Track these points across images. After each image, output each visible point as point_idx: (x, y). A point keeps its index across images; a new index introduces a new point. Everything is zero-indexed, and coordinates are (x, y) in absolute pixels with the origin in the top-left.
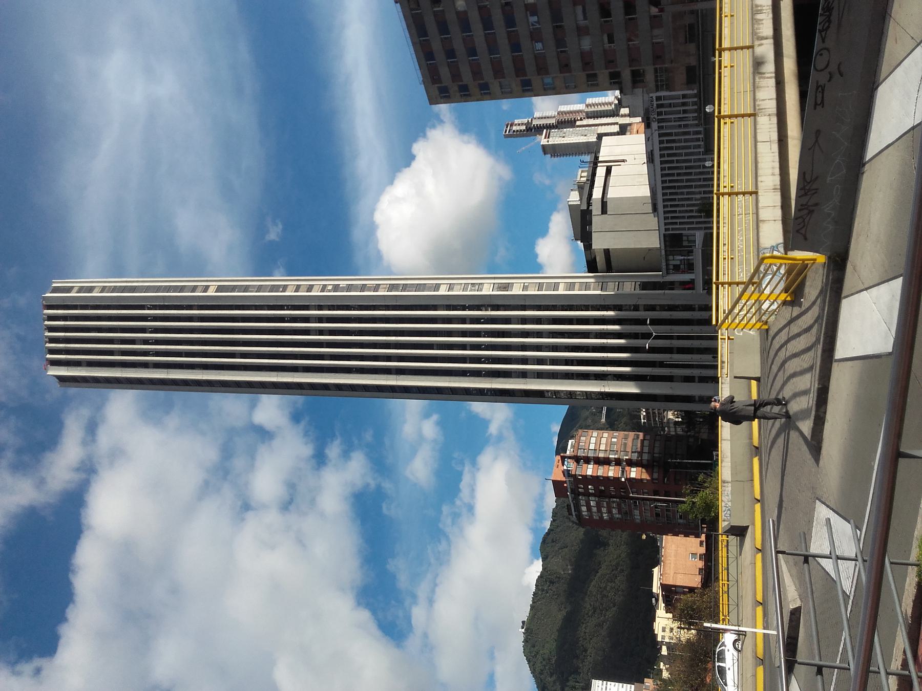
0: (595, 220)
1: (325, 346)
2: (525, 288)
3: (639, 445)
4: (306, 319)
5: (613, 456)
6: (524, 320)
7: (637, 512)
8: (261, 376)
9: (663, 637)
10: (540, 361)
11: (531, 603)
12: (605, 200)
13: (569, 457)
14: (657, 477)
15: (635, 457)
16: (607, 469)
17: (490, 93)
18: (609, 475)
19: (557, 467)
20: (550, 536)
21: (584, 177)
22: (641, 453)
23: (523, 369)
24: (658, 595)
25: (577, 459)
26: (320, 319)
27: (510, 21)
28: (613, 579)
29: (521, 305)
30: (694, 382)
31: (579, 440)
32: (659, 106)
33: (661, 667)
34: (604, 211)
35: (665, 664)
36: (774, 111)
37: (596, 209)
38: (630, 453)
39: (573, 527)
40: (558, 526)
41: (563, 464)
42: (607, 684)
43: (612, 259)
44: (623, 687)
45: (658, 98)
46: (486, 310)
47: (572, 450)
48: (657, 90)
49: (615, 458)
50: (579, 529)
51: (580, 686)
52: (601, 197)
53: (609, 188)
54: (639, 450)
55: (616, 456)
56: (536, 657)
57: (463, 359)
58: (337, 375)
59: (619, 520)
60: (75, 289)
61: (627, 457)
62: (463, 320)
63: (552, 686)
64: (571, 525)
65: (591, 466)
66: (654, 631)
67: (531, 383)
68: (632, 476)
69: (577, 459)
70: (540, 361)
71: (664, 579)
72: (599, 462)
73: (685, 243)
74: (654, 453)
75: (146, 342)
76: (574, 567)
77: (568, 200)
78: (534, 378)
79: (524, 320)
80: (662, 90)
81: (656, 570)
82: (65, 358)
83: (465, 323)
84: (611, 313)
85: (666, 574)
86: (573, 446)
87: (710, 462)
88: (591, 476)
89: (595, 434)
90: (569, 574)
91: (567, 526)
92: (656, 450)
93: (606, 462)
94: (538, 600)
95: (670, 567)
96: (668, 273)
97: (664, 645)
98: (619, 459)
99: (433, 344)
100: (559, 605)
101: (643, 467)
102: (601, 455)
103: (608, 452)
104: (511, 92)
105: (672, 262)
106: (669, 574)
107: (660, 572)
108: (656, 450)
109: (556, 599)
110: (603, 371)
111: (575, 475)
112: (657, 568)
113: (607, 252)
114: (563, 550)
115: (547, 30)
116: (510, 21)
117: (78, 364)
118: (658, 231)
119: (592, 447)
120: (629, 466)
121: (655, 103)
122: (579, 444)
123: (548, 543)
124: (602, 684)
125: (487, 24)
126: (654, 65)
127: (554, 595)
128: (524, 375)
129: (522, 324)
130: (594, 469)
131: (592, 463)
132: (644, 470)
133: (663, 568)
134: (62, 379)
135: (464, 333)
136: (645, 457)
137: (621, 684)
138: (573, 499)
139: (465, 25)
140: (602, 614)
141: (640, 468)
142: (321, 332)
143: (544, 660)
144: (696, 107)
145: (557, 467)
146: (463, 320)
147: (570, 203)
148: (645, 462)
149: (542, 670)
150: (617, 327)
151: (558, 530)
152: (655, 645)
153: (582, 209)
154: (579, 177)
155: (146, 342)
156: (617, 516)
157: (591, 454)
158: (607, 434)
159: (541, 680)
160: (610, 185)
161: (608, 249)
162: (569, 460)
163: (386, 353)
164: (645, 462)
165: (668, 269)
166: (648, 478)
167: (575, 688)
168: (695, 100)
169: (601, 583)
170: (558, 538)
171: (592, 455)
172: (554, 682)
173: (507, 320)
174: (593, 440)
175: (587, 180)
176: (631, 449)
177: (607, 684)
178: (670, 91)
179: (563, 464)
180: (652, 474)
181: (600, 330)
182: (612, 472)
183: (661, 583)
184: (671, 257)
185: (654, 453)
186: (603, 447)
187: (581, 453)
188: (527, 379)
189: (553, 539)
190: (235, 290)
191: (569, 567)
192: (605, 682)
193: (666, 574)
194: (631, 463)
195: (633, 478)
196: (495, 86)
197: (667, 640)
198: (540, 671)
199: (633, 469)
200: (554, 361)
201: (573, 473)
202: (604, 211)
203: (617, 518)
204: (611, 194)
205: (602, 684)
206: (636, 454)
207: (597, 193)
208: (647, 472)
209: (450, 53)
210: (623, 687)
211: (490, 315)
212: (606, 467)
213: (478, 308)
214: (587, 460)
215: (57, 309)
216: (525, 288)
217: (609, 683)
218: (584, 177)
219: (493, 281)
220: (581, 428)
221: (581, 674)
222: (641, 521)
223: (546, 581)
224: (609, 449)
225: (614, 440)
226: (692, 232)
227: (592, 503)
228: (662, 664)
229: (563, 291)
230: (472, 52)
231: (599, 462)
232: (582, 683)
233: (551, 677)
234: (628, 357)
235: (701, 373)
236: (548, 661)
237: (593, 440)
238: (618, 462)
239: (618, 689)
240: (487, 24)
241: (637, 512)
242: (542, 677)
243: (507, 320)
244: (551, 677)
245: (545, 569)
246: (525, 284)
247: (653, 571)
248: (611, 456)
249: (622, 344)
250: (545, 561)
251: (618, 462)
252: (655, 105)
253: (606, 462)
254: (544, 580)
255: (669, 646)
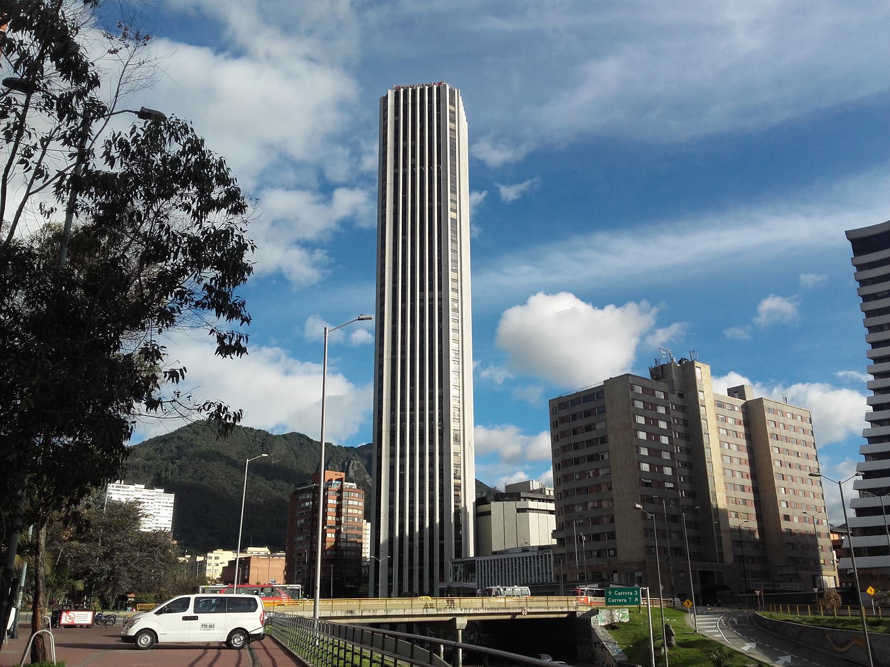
0: (512, 503)
1: (412, 304)
2: (456, 454)
3: (352, 540)
4: (431, 289)
5: (343, 519)
6: (432, 454)
7: (301, 538)
8: (389, 256)
9: (211, 558)
10: (402, 467)
11: (243, 426)
12: (527, 511)
13: (342, 485)
14: (328, 554)
15: (343, 536)
16: (333, 515)
17: (555, 441)
18: (328, 517)
19: (335, 475)
20: (306, 441)
21: (550, 493)
22: (346, 541)
23: (396, 455)
24: (246, 552)
25: (340, 491)
26: (431, 300)
27: (591, 458)
28: (267, 503)
29: (443, 452)
30: (389, 582)
31: (355, 492)
32: (546, 556)
33: (187, 556)
34: (519, 510)
35: (189, 559)
36: (332, 616)
37: (521, 504)
38: (345, 532)
39: (315, 463)
40: (316, 449)
41: (337, 480)
42: (171, 507)
43: (485, 517)
44: (169, 521)
45: (550, 556)
46: (439, 426)
47: (348, 487)
48: (554, 555)
49: (341, 521)
50: (313, 469)
51: (169, 475)
52: (529, 507)
53: (537, 514)
54: (349, 540)
55: (343, 522)
56: (194, 432)
57: (403, 409)
58: (391, 314)
59: (295, 524)
60: (452, 108)
61: (342, 530)
62: (432, 408)
63: (167, 449)
64: (317, 460)
65: (335, 502)
66: (216, 550)
67: (386, 462)
68: (328, 534)
69: (340, 491)
70: (402, 467)
71: (255, 559)
72: (339, 508)
73: (470, 576)
74: (346, 551)
75: (414, 166)
76: (278, 465)
77: (534, 480)
78: (390, 463)
79: (432, 454)
80: (554, 559)
81: (265, 550)
82: (400, 104)
83: (429, 410)
84: (438, 520)
85: (259, 561)
86: (350, 487)
87: (332, 595)
88: (327, 502)
89: (361, 504)
90: (271, 461)
91: (315, 458)
92: (349, 553)
93: (339, 514)
94: (246, 433)
95: (264, 564)
96: (453, 563)
97: (204, 559)
98: (341, 524)
99: (414, 386)
100: (242, 453)
101: (335, 543)
102: (344, 510)
103: (347, 515)
104: (555, 456)
105: (213, 600)
106: (258, 563)
107: (260, 556)
108: (349, 553)
109: (248, 449)
110: (396, 515)
111: (328, 490)
112: (268, 550)
113: (489, 513)
114: (293, 455)
115: (585, 483)
116: (591, 458)
117: (397, 113)
118: (516, 547)
119: (350, 502)
120: (336, 531)
121: (547, 554)
122: (351, 492)
123: (299, 439)
124: (171, 503)
125: (590, 443)
126: (567, 553)
127: (251, 447)
128: (392, 455)
129: (429, 452)
130: (333, 505)
131: (338, 503)
132: (333, 544)
133: (263, 558)
134: (386, 98)
135: (422, 409)
136: (343, 545)
137: (171, 519)
138: (311, 488)
139: (589, 428)
140: (235, 493)
141: (334, 541)
142: (422, 300)
143: (191, 440)
144: (537, 581)
145: (335, 475)
146: (432, 408)
147: (531, 482)
148: (339, 544)
149: (181, 439)
150: (427, 525)
151: (312, 449)
152: (204, 551)
153: (521, 493)
154: (549, 489)
155: (414, 166)
156: (299, 523)
157: (344, 502)
158: (361, 513)
159: (172, 438)
160: (539, 514)
161: (491, 514)
162: (340, 485)
163: (407, 350)
164: (339, 544)
165: (456, 563)
166: (326, 548)
167: (166, 471)
168: (541, 581)
169: (263, 492)
170: (304, 449)
171: (343, 503)
172: (171, 451)
173: (432, 442)
174: (356, 503)
175: (547, 496)
176: (349, 533)
177: (171, 507)
178: (553, 564)
179: (337, 480)
180: (330, 550)
181: (426, 512)
182: (331, 519)
183: (251, 557)
184: (462, 565)
185: (346, 551)
186: (350, 511)
187: (345, 494)
188: (389, 458)
189: (303, 444)
190: (453, 233)
191: (277, 461)
192: (173, 505)
193: (259, 561)
194: (338, 533)
195: (326, 535)
196: (558, 446)
197: (209, 561)
198: (181, 436)
199: (333, 535)
200: (402, 477)
201: (329, 489)
202: (519, 510)
203: (297, 523)
204: (531, 515)
205: (171, 503)
206: (345, 537)
207: (532, 504)
208: (332, 546)
209: (574, 417)
210: (169, 521)
211: (435, 428)
212: (335, 514)
213: (441, 419)
214: (340, 499)
215: (437, 96)
216: (456, 454)
217: (172, 509)
218: (550, 493)
219: (462, 429)
220: (365, 493)
221: (179, 476)
222: (295, 542)
223: (264, 440)
224: (349, 515)
225: (356, 519)
226: (476, 580)
227: (307, 504)
228: (189, 556)
229: (454, 483)
230: (575, 432)
231: (339, 508)
232: (171, 477)
233: (175, 447)
234: (406, 534)
235: (436, 580)
236: (190, 444)
237: (356, 503)
238: (339, 523)
239: (167, 517)
240: (590, 443)
241: (301, 538)
242: (176, 439)
243: (432, 442)
244: (175, 447)
245: (275, 438)
246: (459, 454)
247: (221, 575)
248: (343, 517)
249: (415, 529)
250: (283, 437)
251: (339, 523)
252: (546, 554)
253: (339, 514)
254: (265, 438)
255: (204, 563)
